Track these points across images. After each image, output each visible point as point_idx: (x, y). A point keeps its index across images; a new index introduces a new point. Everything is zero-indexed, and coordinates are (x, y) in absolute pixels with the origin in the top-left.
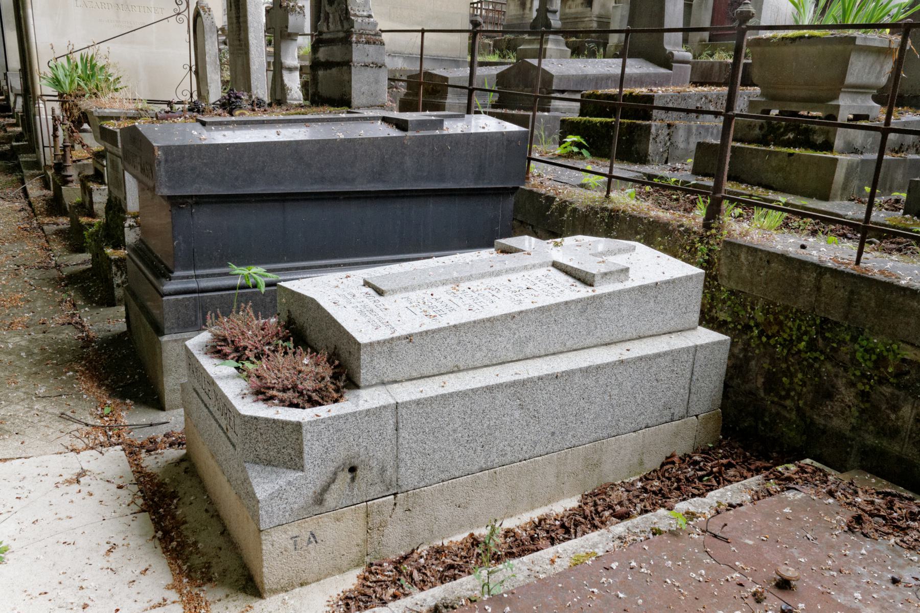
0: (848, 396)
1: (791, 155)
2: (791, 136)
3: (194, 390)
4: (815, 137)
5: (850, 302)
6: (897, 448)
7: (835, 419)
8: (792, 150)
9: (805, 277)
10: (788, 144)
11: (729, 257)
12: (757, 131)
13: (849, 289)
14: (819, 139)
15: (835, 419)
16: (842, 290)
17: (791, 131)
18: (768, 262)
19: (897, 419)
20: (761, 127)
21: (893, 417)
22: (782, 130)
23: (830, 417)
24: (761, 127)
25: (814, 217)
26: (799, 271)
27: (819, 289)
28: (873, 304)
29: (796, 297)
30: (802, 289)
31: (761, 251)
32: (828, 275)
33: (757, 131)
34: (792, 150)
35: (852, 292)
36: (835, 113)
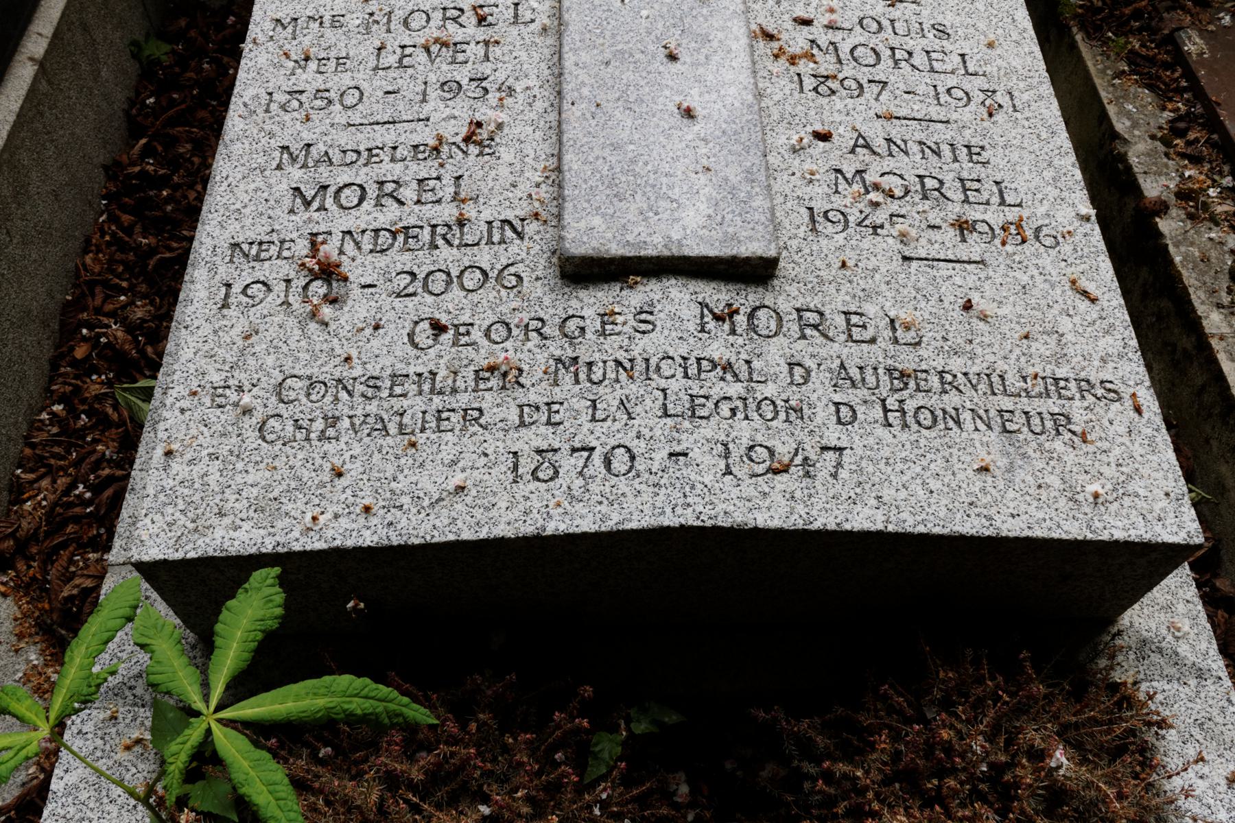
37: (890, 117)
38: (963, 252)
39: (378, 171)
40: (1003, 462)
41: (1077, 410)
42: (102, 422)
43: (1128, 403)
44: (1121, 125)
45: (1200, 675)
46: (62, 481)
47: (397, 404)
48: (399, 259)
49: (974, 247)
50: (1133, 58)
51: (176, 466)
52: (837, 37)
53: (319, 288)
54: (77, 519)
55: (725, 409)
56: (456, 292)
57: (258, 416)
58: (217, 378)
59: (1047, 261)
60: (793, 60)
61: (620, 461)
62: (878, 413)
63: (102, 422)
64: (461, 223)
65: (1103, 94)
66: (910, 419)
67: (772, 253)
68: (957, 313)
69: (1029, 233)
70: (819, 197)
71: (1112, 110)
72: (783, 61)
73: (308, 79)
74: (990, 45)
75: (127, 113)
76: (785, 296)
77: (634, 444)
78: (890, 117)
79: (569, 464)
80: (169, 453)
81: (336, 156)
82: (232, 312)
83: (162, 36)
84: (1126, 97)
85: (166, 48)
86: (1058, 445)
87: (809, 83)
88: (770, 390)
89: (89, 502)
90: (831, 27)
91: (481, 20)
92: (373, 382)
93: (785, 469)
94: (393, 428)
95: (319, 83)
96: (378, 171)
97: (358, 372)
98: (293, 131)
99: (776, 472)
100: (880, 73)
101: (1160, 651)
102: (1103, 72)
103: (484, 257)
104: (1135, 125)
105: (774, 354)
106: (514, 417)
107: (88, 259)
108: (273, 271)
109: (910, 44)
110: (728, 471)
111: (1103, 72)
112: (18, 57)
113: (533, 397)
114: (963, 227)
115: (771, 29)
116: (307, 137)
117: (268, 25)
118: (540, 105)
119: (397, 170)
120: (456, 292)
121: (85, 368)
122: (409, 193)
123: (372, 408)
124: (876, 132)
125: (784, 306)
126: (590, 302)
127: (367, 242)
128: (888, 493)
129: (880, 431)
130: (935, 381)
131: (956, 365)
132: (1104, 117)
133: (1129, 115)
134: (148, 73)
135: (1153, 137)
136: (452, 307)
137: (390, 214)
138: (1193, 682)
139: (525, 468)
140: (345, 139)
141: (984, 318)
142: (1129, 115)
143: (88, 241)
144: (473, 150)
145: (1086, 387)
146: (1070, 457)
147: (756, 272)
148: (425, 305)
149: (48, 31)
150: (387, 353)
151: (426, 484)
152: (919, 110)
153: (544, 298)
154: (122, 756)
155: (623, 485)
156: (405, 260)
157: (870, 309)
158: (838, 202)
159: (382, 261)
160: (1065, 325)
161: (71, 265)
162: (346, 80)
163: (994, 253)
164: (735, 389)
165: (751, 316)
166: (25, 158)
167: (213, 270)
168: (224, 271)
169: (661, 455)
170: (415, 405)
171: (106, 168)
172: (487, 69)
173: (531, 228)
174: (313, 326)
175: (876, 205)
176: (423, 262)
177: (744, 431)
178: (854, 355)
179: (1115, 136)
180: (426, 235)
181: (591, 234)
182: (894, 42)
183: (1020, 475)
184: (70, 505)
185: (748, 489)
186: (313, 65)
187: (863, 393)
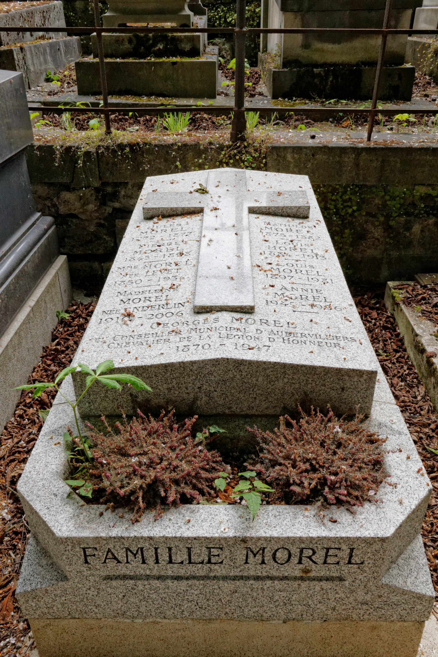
0: (377, 232)
1: (174, 63)
2: (161, 47)
3: (157, 562)
4: (183, 46)
5: (382, 168)
6: (411, 253)
7: (368, 251)
8: (174, 59)
9: (346, 159)
10: (159, 54)
11: (276, 159)
12: (127, 46)
13: (380, 159)
14: (187, 47)
15: (368, 251)
16: (376, 161)
17: (161, 41)
18: (313, 155)
19: (410, 235)
20: (130, 41)
21: (408, 234)
22: (151, 42)
23: (365, 251)
24: (130, 41)
25: (119, 111)
26: (341, 157)
27: (357, 165)
28: (398, 165)
29: (340, 176)
30: (344, 169)
31: (306, 148)
32: (364, 154)
33: (127, 46)
34: (174, 59)
35: (383, 161)
36: (187, 23)
37: (293, 283)
38: (312, 310)
39: (144, 295)
40: (317, 351)
41: (342, 343)
42: (33, 422)
43: (358, 342)
44: (418, 331)
45: (400, 433)
46: (16, 440)
47: (146, 339)
48: (149, 312)
49: (315, 309)
50: (423, 312)
51: (84, 353)
52: (279, 267)
53: (126, 319)
54: (19, 452)
55: (237, 337)
56: (164, 317)
57: (107, 343)
58: (97, 337)
59: (337, 313)
60: (265, 271)
61: (206, 347)
62: (282, 340)
63: (33, 422)
64: (167, 304)
65: (412, 323)
66: (291, 342)
67: (252, 304)
68: (309, 322)
69: (333, 308)
70: (269, 298)
71: (415, 327)
72: (262, 272)
73: (127, 278)
74: (326, 270)
75: (52, 333)
76: (257, 317)
77: (211, 344)
78: (293, 283)
79: (192, 348)
80: (83, 351)
81: (133, 293)
82: (102, 324)
83: (67, 312)
84: (421, 323)
85: (68, 315)
86: (335, 349)
87: (269, 276)
88: (250, 334)
89: (25, 447)
90: (277, 265)
91: (176, 265)
92: (140, 336)
93: (252, 349)
94: (144, 344)
95: (130, 279)
96: (144, 295)
97: (136, 333)
98: (122, 289)
99: (250, 349)
100: (291, 274)
101: (386, 426)
102: (412, 316)
103: (173, 310)
104: (424, 331)
105: (252, 328)
106: (178, 340)
107: (34, 374)
108: (114, 316)
109: (301, 269)
110: (236, 348)
111: (412, 316)
112: (26, 305)
113: (183, 336)
114: (312, 306)
115: (260, 264)
116: (125, 290)
117: (116, 269)
118: (191, 281)
119: (150, 295)
120: (164, 317)
121: (30, 406)
122: (153, 299)
123: (139, 340)
124: (289, 286)
125: (256, 318)
126: (201, 318)
127: (140, 309)
128: (281, 355)
129: (281, 344)
130: (299, 335)
131: (306, 332)
132: (413, 330)
133: (422, 328)
134: (62, 322)
135: (431, 335)
136: (162, 320)
137: (148, 303)
138: (397, 436)
139: (180, 349)
140: (136, 290)
141: (316, 323)
142: (422, 328)
143: (34, 369)
144: (172, 290)
145: (345, 338)
146: (338, 352)
147: (248, 310)
148: (157, 320)
149: (36, 299)
150: (146, 329)
151: (153, 353)
152: (302, 282)
153: (190, 317)
154: (53, 446)
155: (206, 351)
156: (152, 312)
157: (281, 320)
158: (275, 299)
159: (144, 312)
160: (341, 326)
161: (28, 375)
162: (138, 278)
163: (322, 312)
164: (240, 333)
165: (246, 320)
166: (22, 333)
167: (98, 316)
168: (100, 317)
169: (218, 345)
170: (151, 339)
171: (43, 348)
172: (177, 274)
173: (186, 304)
174: (124, 326)
175: (286, 300)
176: (156, 312)
177: (241, 341)
178: (275, 329)
179: (417, 335)
180: (157, 307)
181: (203, 300)
182: (296, 268)
183: (322, 354)
184: (18, 447)
185: (241, 352)
186: (128, 276)
187: (277, 336)
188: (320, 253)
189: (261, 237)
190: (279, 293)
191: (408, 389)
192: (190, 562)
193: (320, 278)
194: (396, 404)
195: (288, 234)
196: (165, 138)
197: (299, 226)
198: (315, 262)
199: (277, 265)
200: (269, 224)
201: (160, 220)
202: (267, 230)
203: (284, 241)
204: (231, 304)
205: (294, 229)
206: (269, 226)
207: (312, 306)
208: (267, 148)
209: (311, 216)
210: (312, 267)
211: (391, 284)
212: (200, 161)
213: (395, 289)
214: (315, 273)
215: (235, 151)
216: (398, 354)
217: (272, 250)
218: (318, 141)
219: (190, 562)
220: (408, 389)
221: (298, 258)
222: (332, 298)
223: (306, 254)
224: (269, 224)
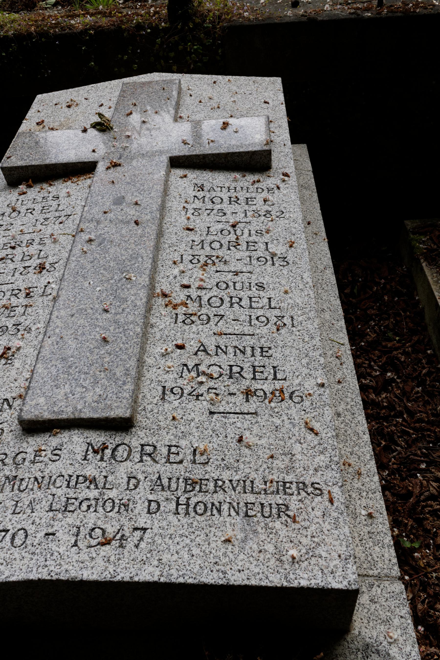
43: (326, 496)
72: (170, 308)
90: (200, 288)
101: (378, 652)
114: (248, 394)
125: (135, 443)
126: (34, 443)
128: (166, 557)
181: (39, 407)
188: (279, 249)
189: (182, 221)
190: (191, 364)
191: (426, 398)
192: (270, 307)
193: (272, 314)
194: (401, 579)
195: (229, 209)
196: (73, 22)
197: (251, 189)
198: (267, 274)
199: (200, 288)
200: (202, 188)
201: (29, 186)
202: (198, 204)
203: (220, 226)
204: (87, 414)
205: (242, 195)
206: (200, 194)
207: (248, 394)
208: (223, 29)
209: (274, 164)
210: (261, 287)
211: (409, 224)
212: (126, 57)
213: (414, 233)
214: (266, 301)
215: (176, 38)
216: (415, 338)
217: (197, 250)
218: (301, 12)
219: (270, 307)
220: (426, 398)
221: (239, 267)
222: (287, 368)
223: (255, 255)
224: (202, 188)
